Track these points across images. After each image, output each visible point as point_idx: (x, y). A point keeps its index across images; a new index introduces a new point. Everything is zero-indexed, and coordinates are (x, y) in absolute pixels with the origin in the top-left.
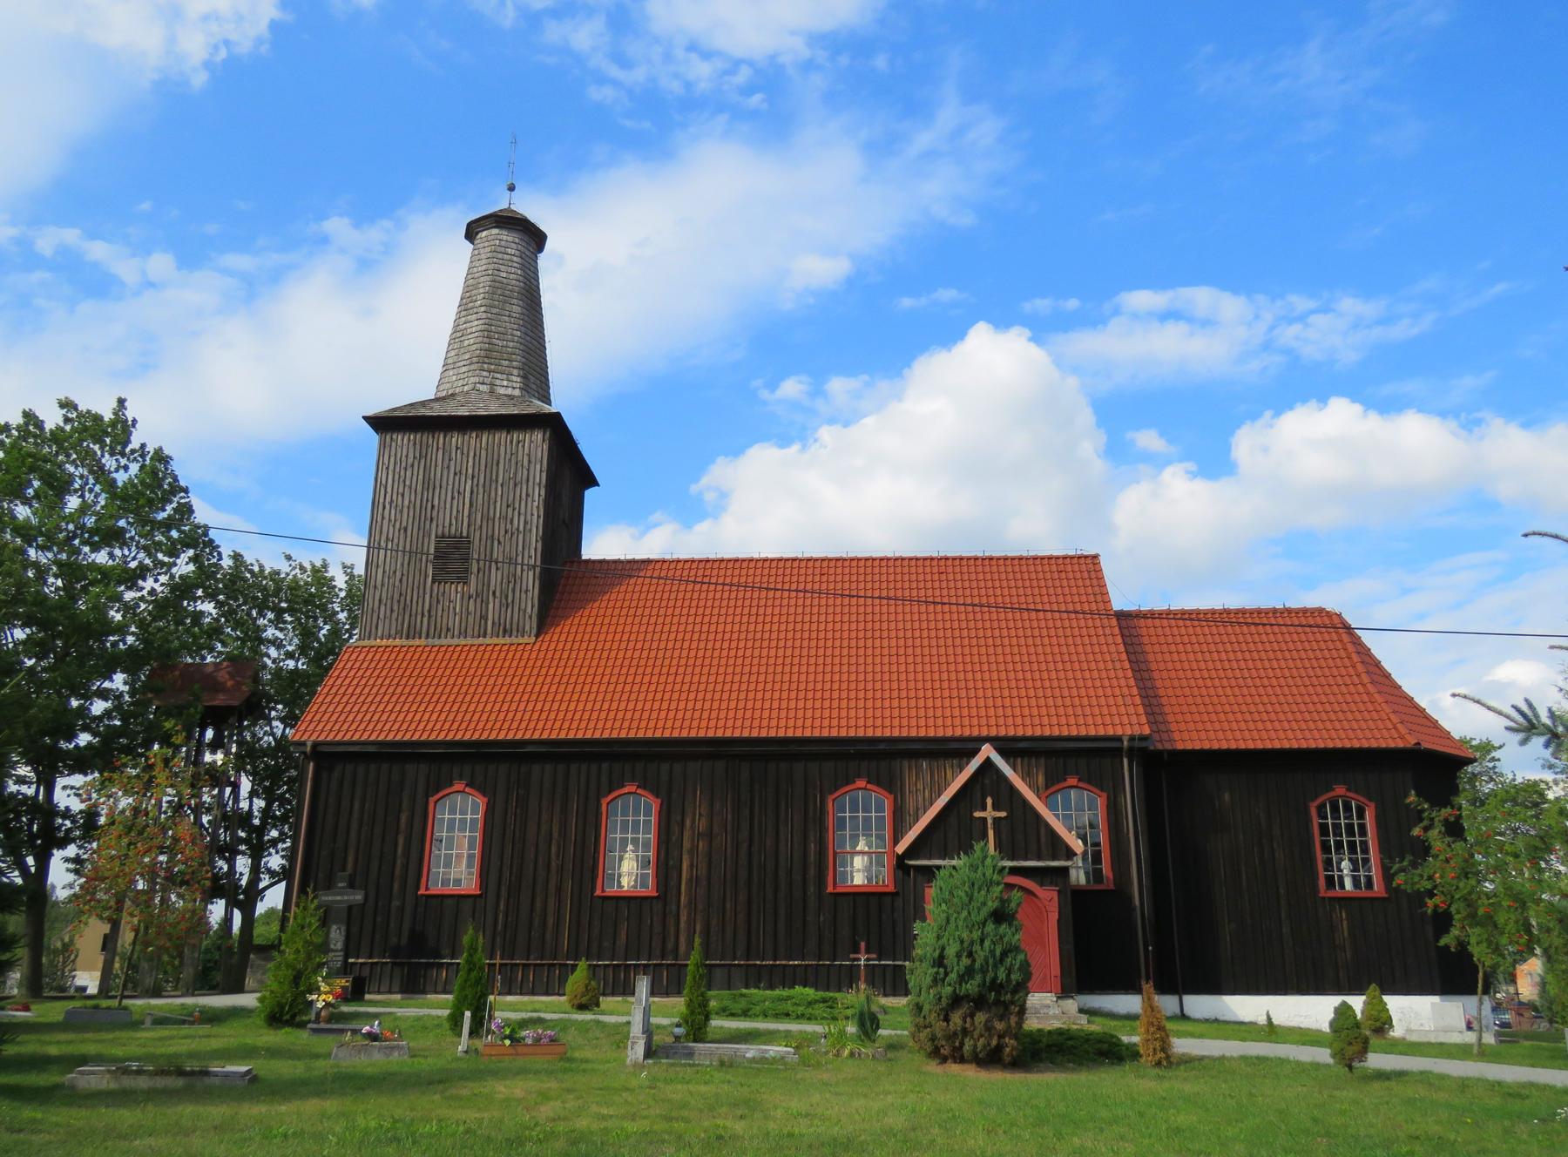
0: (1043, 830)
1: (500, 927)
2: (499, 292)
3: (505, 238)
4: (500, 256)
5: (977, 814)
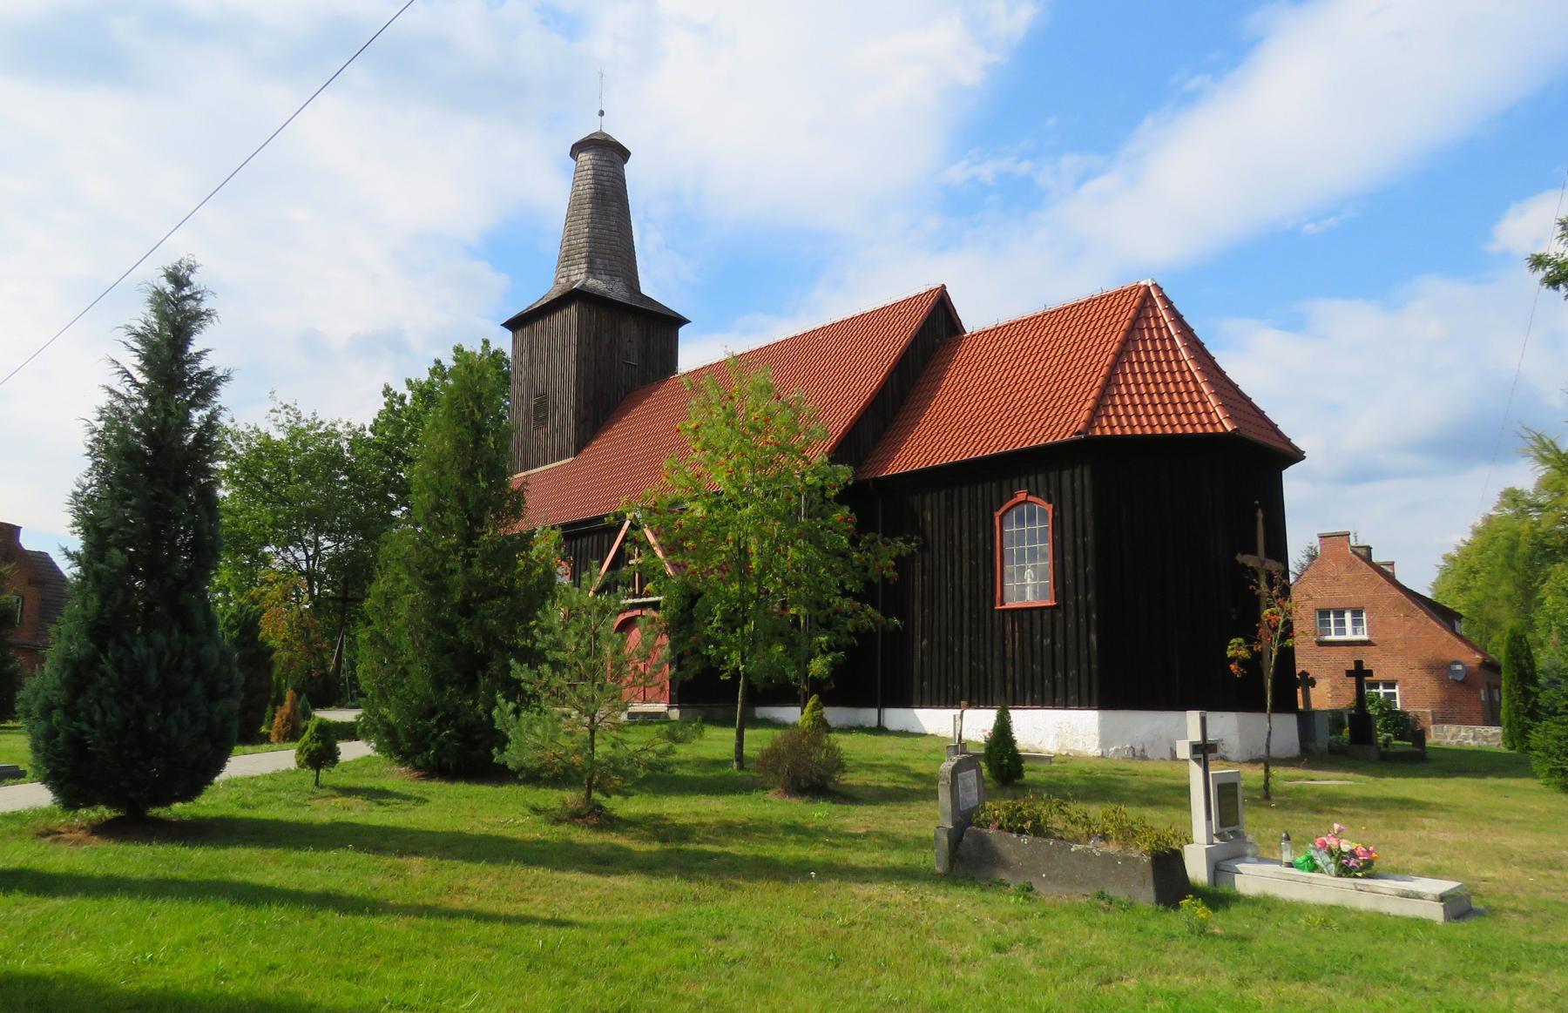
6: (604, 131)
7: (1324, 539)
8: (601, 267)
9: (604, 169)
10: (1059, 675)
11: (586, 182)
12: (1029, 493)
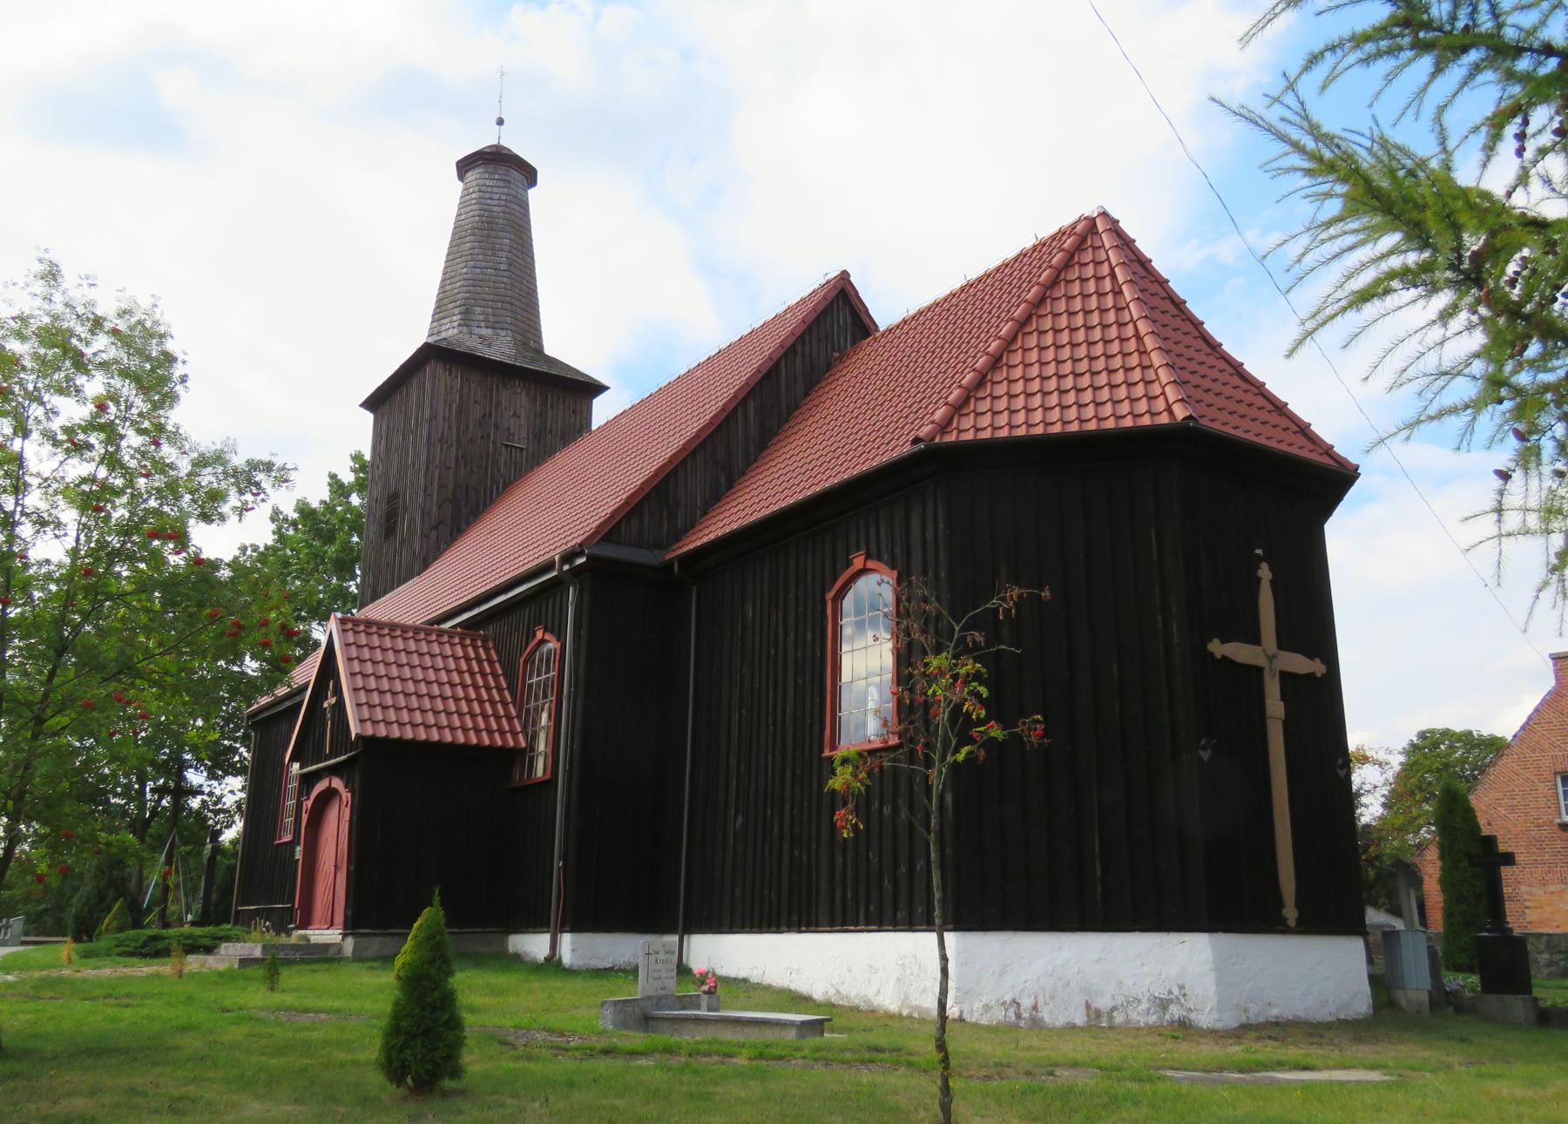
1: (790, 747)
6: (502, 143)
7: (1561, 662)
8: (481, 317)
9: (495, 190)
10: (903, 869)
12: (868, 557)
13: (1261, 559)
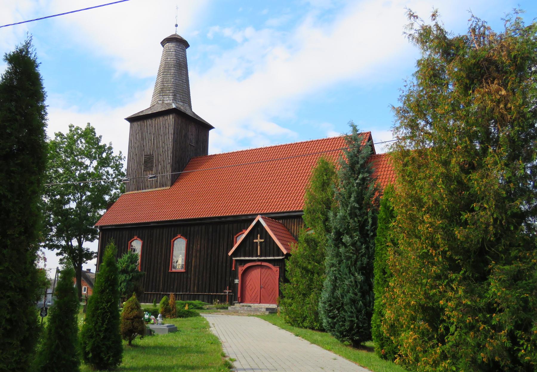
0: (275, 246)
1: (145, 282)
2: (167, 66)
3: (170, 46)
4: (168, 53)
5: (255, 241)
6: (178, 33)
8: (179, 98)
9: (180, 52)
11: (171, 57)
13: (80, 243)
